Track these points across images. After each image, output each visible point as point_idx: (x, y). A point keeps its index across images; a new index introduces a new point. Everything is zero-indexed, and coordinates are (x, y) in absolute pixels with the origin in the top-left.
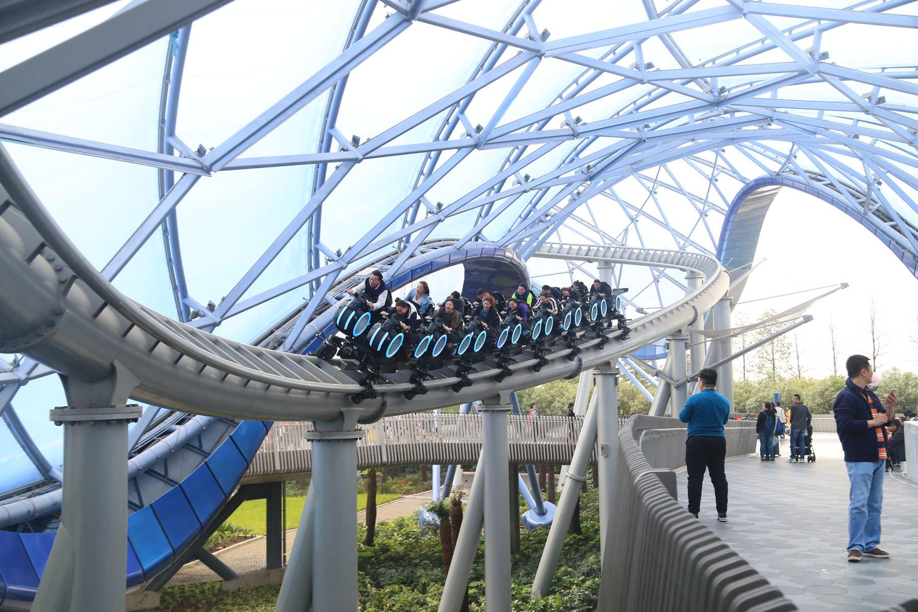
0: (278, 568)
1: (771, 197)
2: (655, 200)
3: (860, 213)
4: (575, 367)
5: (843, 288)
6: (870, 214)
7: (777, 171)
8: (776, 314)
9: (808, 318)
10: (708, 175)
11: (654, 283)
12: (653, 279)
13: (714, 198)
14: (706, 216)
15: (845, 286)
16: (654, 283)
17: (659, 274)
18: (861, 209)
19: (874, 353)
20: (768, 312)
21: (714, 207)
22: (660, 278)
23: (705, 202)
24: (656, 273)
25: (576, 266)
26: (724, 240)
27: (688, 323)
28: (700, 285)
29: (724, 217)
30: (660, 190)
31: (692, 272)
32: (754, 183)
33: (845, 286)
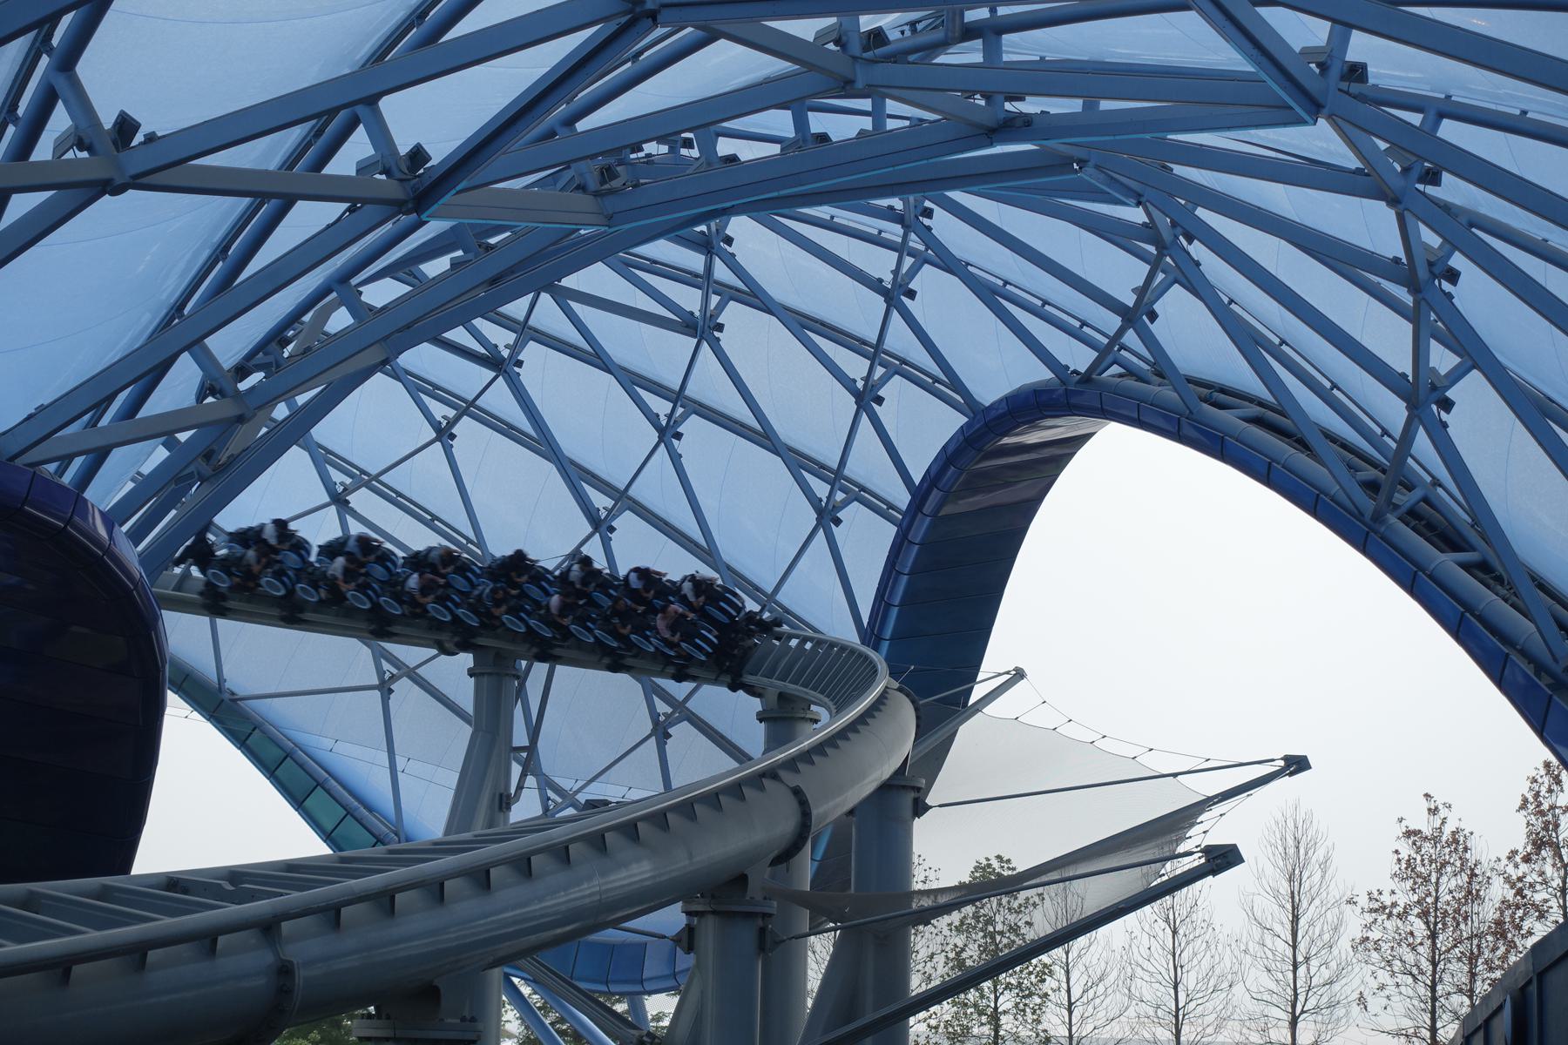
0: (1019, 873)
1: (1061, 453)
2: (676, 458)
3: (1359, 515)
4: (261, 982)
5: (1291, 774)
6: (1392, 519)
7: (1083, 370)
8: (1010, 873)
9: (1224, 855)
10: (855, 381)
11: (653, 739)
12: (649, 727)
13: (870, 464)
14: (838, 522)
15: (1296, 764)
16: (653, 739)
17: (669, 710)
18: (1367, 504)
19: (1294, 1006)
20: (989, 866)
21: (861, 494)
22: (672, 725)
23: (836, 477)
24: (662, 707)
25: (405, 670)
26: (889, 606)
27: (772, 856)
28: (825, 722)
29: (892, 530)
30: (694, 427)
31: (783, 697)
32: (1003, 408)
33: (1296, 764)
